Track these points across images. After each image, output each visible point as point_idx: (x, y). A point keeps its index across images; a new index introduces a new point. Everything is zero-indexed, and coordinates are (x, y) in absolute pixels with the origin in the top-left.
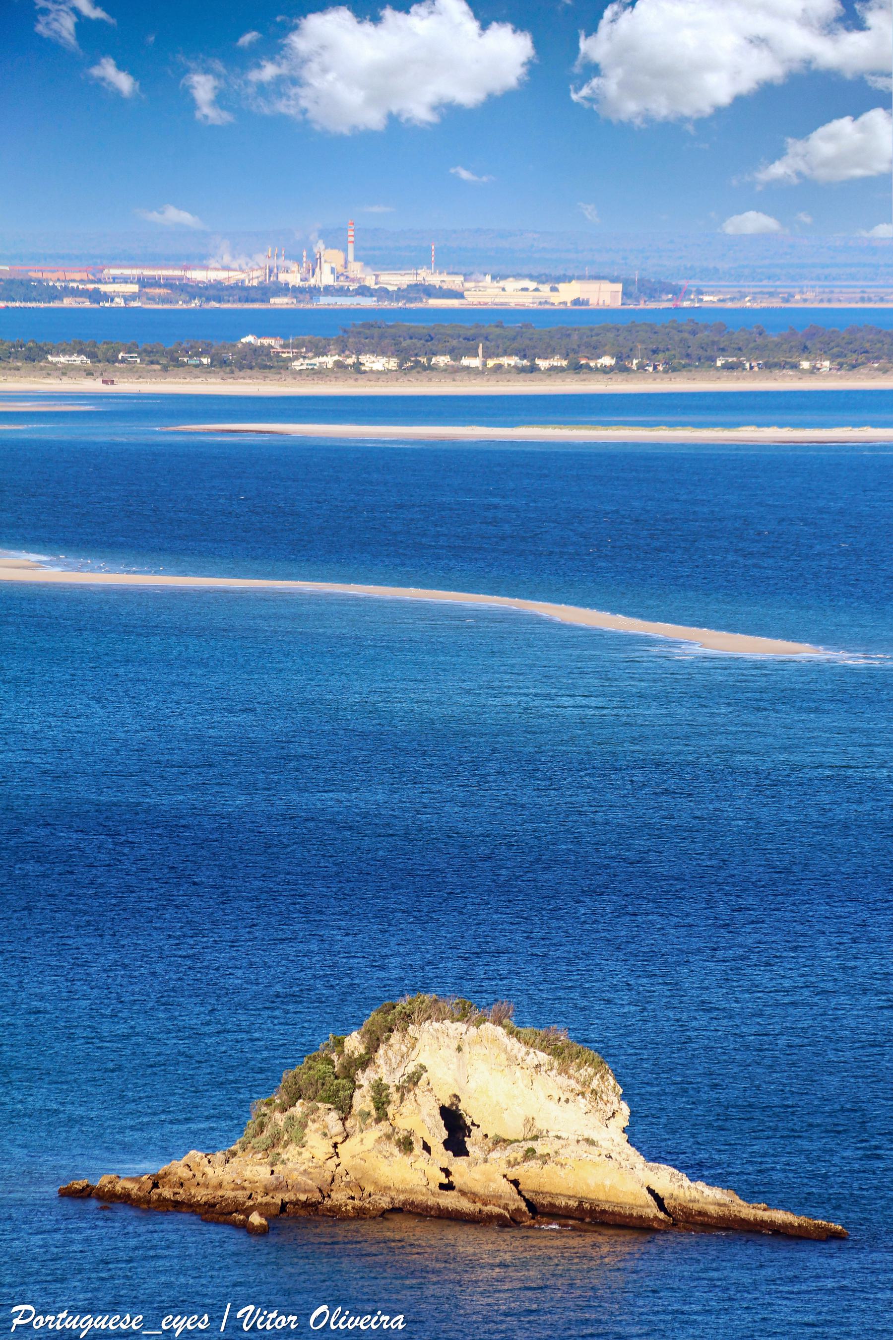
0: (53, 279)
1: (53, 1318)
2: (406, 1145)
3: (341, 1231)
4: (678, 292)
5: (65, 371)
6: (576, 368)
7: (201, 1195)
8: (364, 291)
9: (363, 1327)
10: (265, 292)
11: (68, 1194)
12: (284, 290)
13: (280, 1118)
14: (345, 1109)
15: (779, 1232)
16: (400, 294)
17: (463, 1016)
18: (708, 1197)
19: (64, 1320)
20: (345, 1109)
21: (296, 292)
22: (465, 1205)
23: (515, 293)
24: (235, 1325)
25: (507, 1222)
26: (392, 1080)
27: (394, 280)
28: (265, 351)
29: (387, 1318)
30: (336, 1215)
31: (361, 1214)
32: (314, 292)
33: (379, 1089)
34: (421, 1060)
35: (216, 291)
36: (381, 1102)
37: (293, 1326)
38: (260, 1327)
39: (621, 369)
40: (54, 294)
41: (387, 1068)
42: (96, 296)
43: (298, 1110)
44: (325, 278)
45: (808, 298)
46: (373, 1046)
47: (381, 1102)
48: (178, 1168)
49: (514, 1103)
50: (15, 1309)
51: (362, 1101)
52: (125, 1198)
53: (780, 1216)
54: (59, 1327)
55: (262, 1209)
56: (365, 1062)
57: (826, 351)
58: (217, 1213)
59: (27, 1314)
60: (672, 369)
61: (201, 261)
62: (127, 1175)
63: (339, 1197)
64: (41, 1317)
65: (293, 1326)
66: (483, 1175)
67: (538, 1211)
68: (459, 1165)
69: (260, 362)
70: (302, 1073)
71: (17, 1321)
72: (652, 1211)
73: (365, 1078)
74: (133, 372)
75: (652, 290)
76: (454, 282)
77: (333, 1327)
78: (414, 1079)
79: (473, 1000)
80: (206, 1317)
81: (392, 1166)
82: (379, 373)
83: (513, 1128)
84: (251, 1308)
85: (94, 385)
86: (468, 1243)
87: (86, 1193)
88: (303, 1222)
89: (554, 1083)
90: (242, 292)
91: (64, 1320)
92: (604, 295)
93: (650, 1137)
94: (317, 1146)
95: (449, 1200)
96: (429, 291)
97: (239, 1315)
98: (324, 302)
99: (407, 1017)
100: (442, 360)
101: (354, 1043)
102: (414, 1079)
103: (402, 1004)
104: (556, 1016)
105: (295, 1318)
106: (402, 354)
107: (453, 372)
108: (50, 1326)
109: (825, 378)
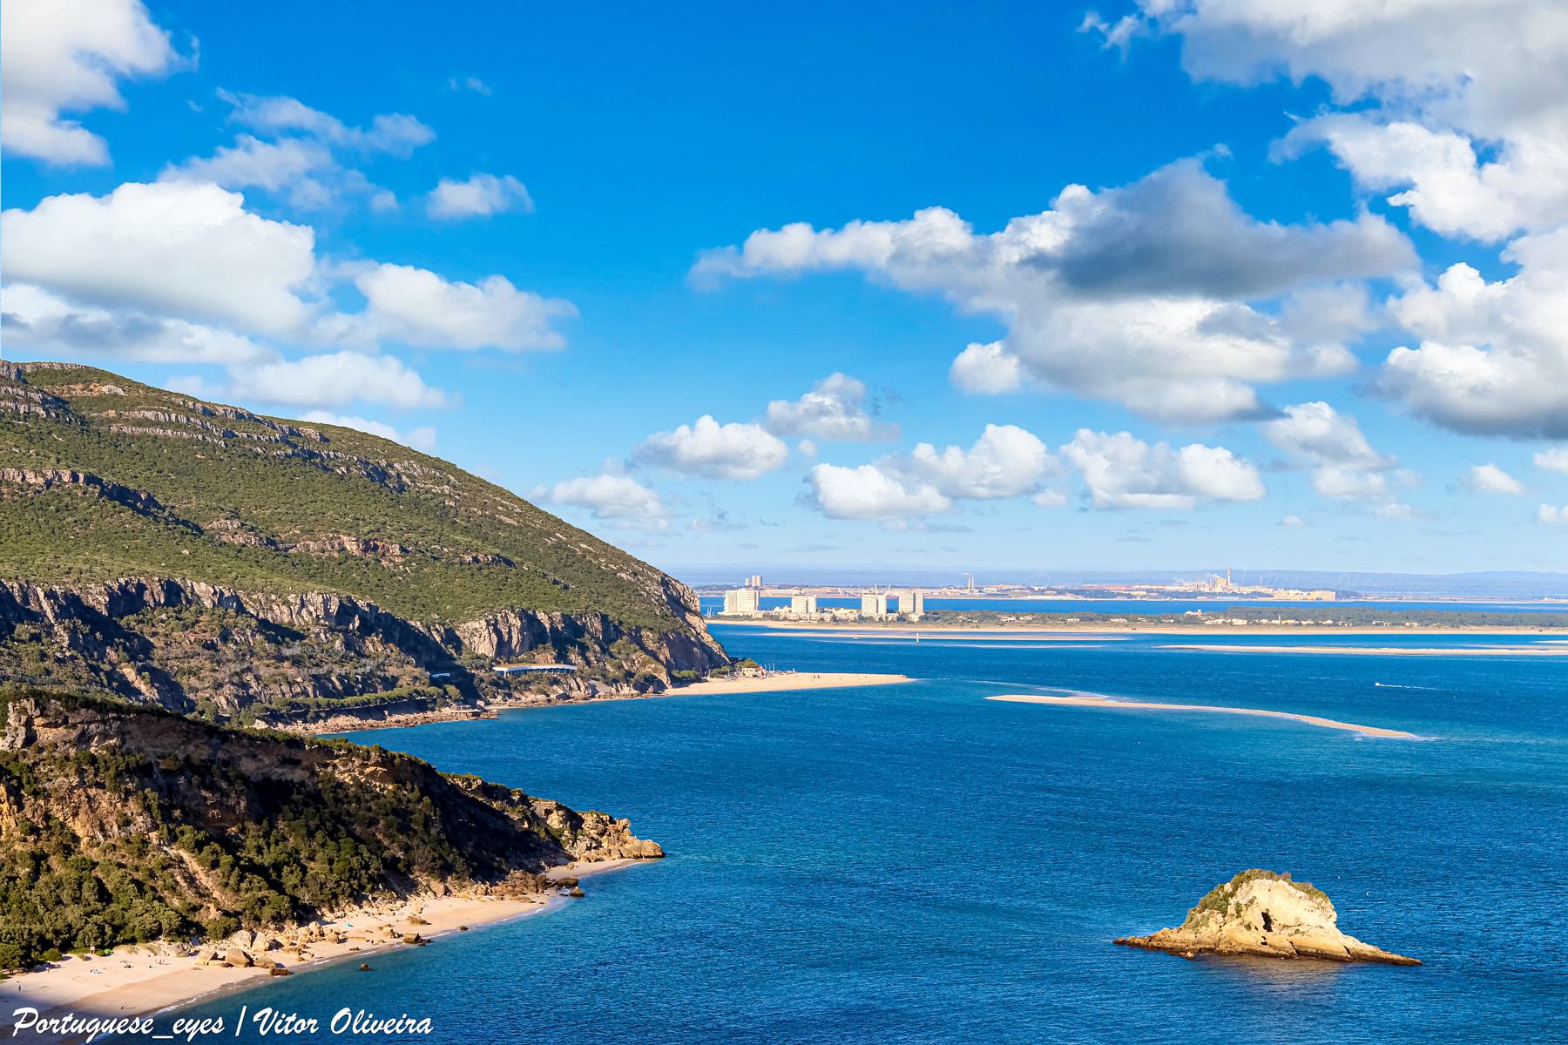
0: (1112, 589)
1: (57, 1022)
2: (1248, 927)
3: (1227, 961)
4: (1357, 595)
5: (1117, 625)
6: (1318, 624)
7: (1168, 945)
8: (1234, 594)
9: (388, 1032)
10: (1195, 594)
11: (1116, 943)
12: (1202, 594)
13: (1199, 916)
14: (1224, 913)
15: (1395, 963)
16: (1248, 595)
17: (1271, 877)
18: (1368, 949)
19: (69, 1024)
20: (1224, 913)
21: (1208, 594)
22: (1272, 951)
23: (1293, 595)
24: (250, 1027)
25: (1288, 957)
26: (1243, 902)
27: (1247, 590)
28: (1194, 617)
29: (413, 1022)
30: (1220, 953)
31: (1230, 953)
32: (1214, 594)
33: (1238, 905)
34: (1255, 893)
35: (1176, 594)
36: (1238, 912)
37: (313, 1031)
38: (356, 1031)
39: (1335, 625)
40: (1113, 595)
41: (1241, 897)
42: (1129, 596)
43: (1206, 913)
44: (1218, 589)
45: (1408, 598)
46: (1236, 888)
47: (1238, 912)
48: (1159, 934)
49: (1286, 911)
50: (17, 1012)
51: (1231, 910)
52: (1139, 945)
53: (1396, 957)
54: (64, 1032)
55: (1192, 951)
56: (1232, 895)
57: (1416, 619)
58: (1174, 952)
59: (30, 1018)
60: (1355, 625)
61: (1171, 583)
62: (1139, 937)
63: (1222, 947)
64: (44, 1021)
65: (313, 1031)
66: (1280, 939)
67: (1302, 954)
68: (1269, 935)
69: (1192, 621)
70: (1208, 898)
71: (18, 1025)
72: (1345, 954)
73: (1232, 901)
74: (1144, 625)
75: (1347, 594)
76: (1270, 591)
77: (356, 1031)
78: (1251, 902)
79: (1275, 867)
80: (220, 1021)
81: (1238, 933)
82: (1240, 626)
83: (1290, 921)
84: (269, 1011)
85: (1128, 630)
86: (1273, 965)
87: (1123, 943)
88: (1208, 956)
89: (1307, 904)
90: (1188, 595)
91: (69, 1024)
92: (1329, 597)
93: (1344, 926)
94: (1214, 927)
95: (1265, 949)
96: (1260, 595)
97: (256, 1019)
98: (1218, 598)
99: (1249, 877)
100: (1264, 621)
101: (1228, 887)
102: (1251, 902)
103: (1247, 872)
104: (1308, 872)
105: (315, 1022)
106: (1248, 618)
107: (1269, 626)
108: (55, 1031)
109: (1416, 629)
